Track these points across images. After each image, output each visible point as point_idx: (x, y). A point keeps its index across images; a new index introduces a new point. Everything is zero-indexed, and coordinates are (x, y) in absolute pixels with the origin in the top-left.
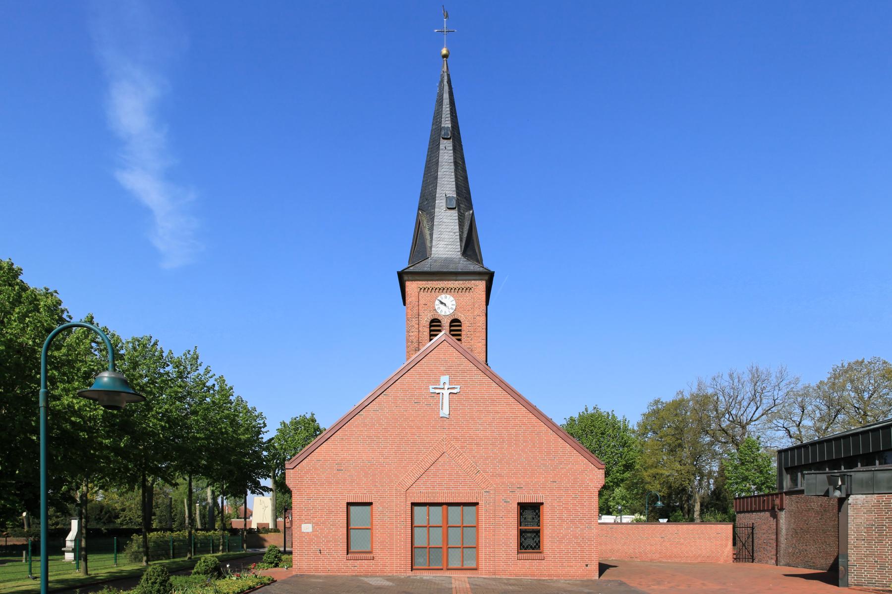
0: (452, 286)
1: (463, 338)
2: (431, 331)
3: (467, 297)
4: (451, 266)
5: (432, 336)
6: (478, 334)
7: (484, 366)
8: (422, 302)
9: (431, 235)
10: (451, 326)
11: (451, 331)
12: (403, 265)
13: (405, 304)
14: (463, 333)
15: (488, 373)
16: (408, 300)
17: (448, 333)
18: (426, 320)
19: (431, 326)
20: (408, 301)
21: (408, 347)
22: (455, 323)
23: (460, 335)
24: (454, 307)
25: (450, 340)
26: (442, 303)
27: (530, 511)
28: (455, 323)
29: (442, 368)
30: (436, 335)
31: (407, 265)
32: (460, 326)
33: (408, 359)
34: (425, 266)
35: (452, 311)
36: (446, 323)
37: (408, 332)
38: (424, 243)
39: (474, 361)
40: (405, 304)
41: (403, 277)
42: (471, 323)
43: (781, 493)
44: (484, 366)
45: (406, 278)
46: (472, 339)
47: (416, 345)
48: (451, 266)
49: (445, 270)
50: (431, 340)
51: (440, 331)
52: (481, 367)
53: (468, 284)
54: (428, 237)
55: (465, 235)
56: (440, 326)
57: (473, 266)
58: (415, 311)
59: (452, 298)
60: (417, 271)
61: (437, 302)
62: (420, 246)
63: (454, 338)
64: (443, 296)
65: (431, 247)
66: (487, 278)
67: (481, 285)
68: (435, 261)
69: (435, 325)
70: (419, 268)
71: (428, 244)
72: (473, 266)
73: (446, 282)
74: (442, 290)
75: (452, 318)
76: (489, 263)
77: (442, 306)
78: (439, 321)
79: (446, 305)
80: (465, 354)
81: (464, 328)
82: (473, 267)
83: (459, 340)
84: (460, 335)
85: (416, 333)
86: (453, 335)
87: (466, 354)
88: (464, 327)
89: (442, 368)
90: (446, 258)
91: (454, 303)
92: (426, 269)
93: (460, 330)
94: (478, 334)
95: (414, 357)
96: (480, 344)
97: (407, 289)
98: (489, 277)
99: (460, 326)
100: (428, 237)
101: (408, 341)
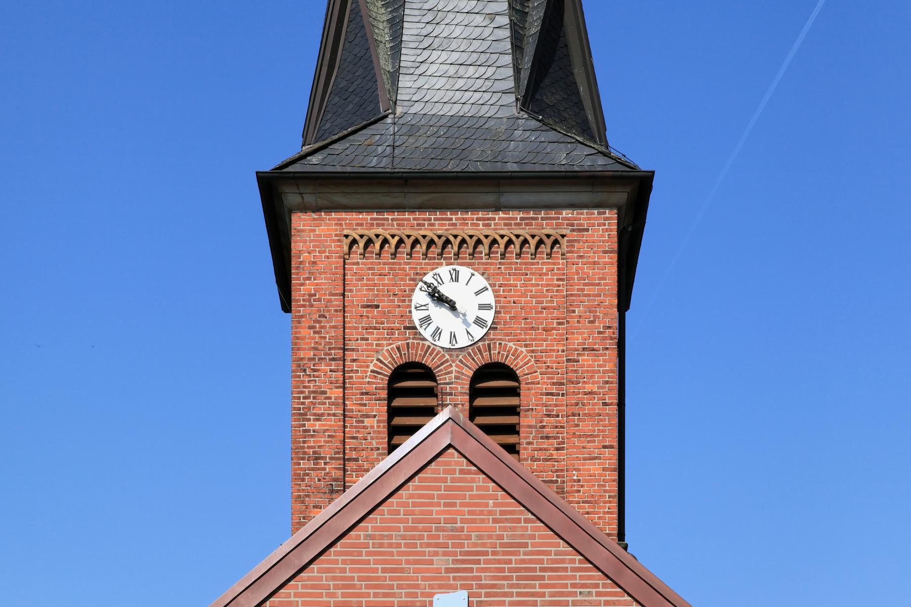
0: (480, 231)
1: (527, 439)
2: (393, 412)
3: (544, 271)
4: (476, 153)
5: (397, 432)
6: (586, 426)
7: (609, 551)
8: (358, 294)
9: (396, 25)
10: (475, 393)
11: (475, 412)
12: (282, 144)
13: (287, 305)
14: (526, 421)
15: (628, 580)
16: (301, 289)
17: (463, 417)
18: (374, 363)
19: (393, 393)
20: (299, 293)
21: (298, 478)
22: (494, 383)
23: (512, 429)
24: (488, 316)
25: (471, 447)
26: (439, 299)
27: (477, 293)
28: (494, 383)
29: (441, 562)
30: (412, 430)
31: (295, 148)
32: (514, 392)
33: (299, 525)
34: (371, 151)
35: (478, 333)
36: (455, 380)
37: (301, 416)
38: (365, 62)
39: (570, 533)
40: (287, 305)
41: (278, 195)
42: (558, 373)
43: (344, 459)
44: (609, 551)
45: (291, 197)
46: (567, 449)
47: (332, 469)
48: (476, 153)
49: (452, 166)
50: (392, 448)
51: (431, 412)
52: (600, 556)
53: (546, 223)
54: (383, 33)
55: (534, 28)
56: (429, 392)
57: (562, 149)
58: (331, 334)
59: (480, 281)
60: (341, 166)
61: (420, 297)
62: (350, 71)
63: (492, 442)
64: (444, 271)
65: (395, 76)
66: (621, 196)
67: (601, 227)
68: (413, 130)
69: (410, 388)
70: (344, 157)
71: (385, 63)
72: (562, 149)
73: (456, 217)
74: (442, 248)
75: (481, 360)
76: (631, 137)
77: (439, 314)
78: (428, 374)
79: (458, 310)
80: (532, 501)
81: (528, 398)
82: (566, 154)
83: (512, 449)
84: (512, 429)
85: (333, 423)
86: (489, 430)
87: (538, 503)
88: (531, 398)
89: (441, 562)
90: (455, 122)
91: (488, 297)
92: (374, 163)
93: (513, 411)
94: (586, 426)
95: (321, 517)
96: (595, 468)
97: (298, 245)
98: (631, 195)
99: (514, 392)
100: (383, 33)
101: (298, 453)
